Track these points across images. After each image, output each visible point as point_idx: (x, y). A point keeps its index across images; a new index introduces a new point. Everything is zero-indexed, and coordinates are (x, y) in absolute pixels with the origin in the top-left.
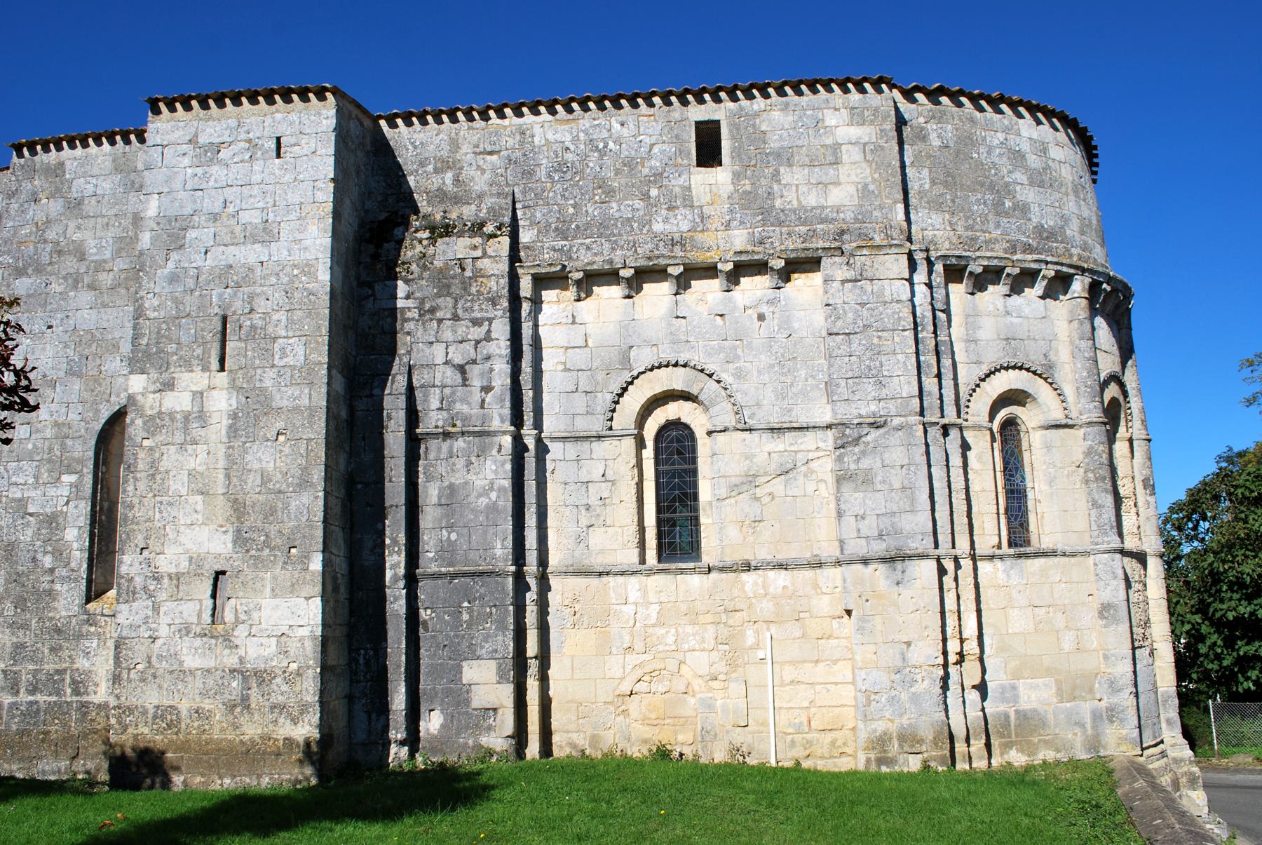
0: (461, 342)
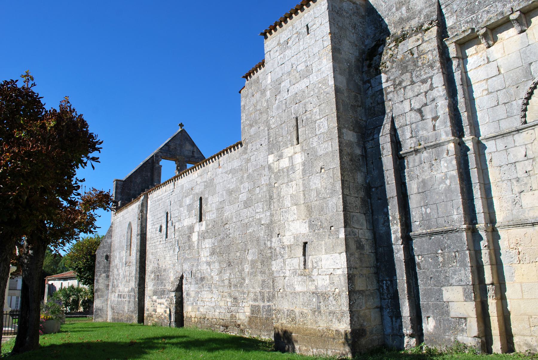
0: (417, 96)
